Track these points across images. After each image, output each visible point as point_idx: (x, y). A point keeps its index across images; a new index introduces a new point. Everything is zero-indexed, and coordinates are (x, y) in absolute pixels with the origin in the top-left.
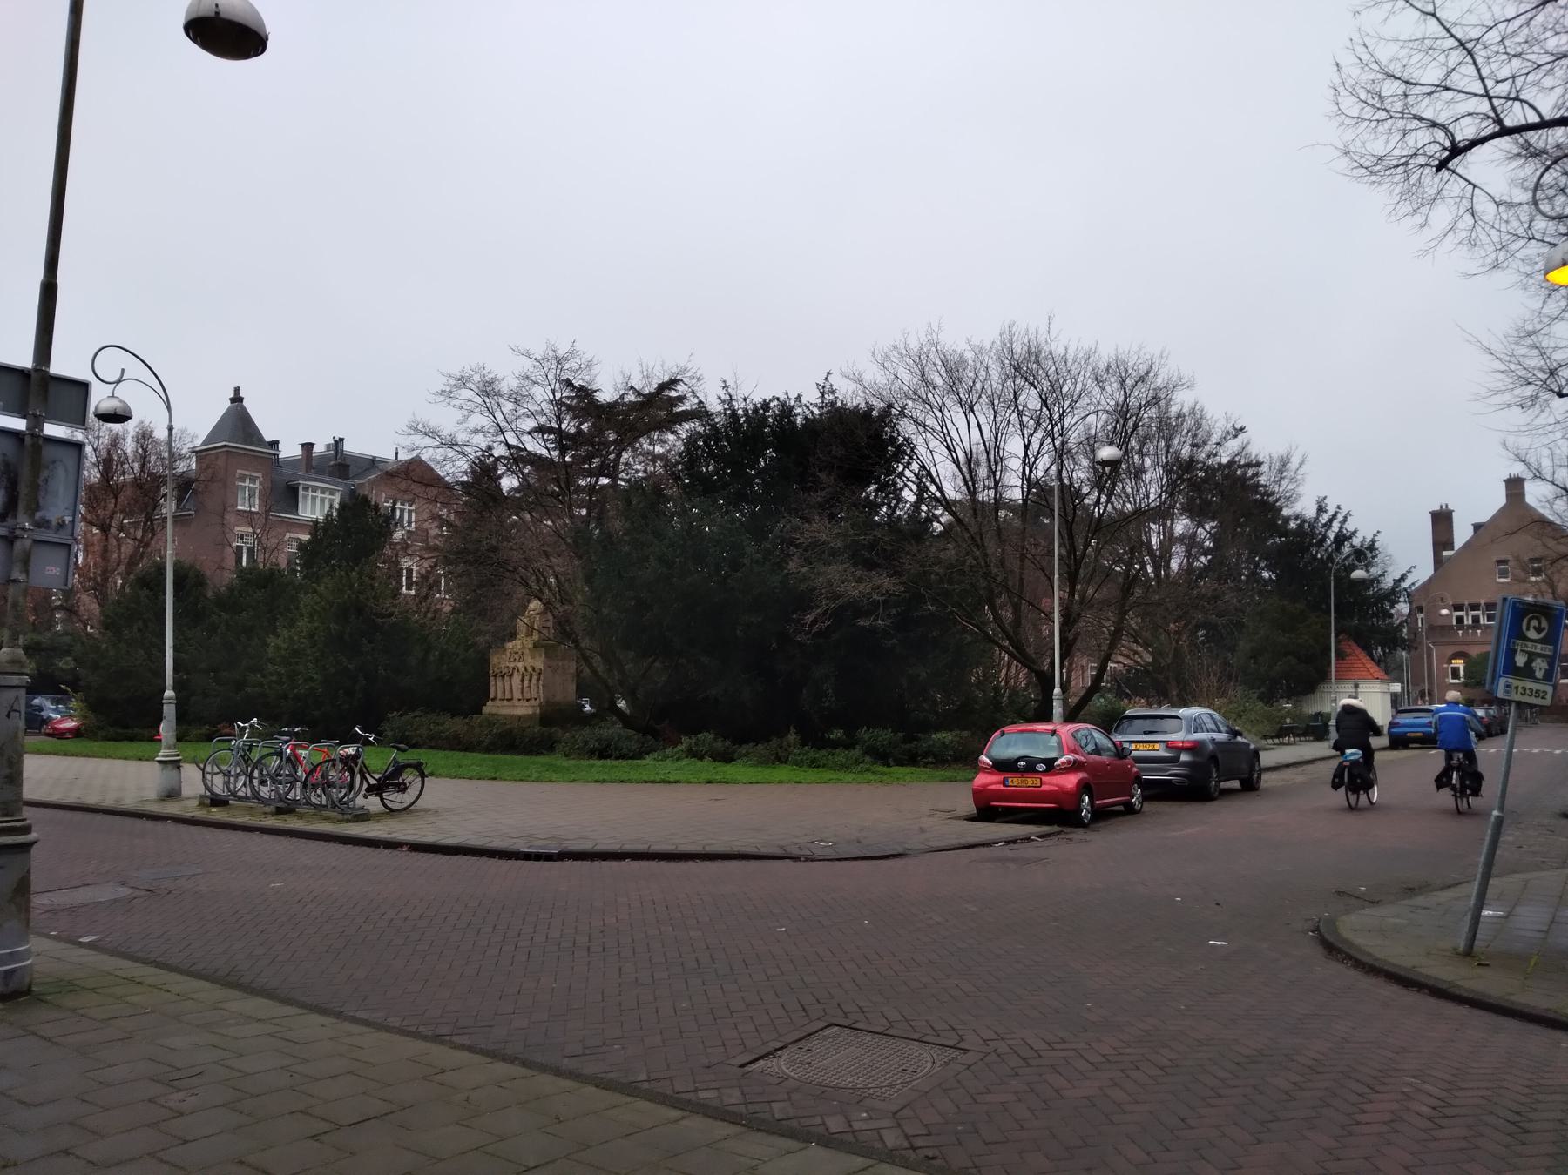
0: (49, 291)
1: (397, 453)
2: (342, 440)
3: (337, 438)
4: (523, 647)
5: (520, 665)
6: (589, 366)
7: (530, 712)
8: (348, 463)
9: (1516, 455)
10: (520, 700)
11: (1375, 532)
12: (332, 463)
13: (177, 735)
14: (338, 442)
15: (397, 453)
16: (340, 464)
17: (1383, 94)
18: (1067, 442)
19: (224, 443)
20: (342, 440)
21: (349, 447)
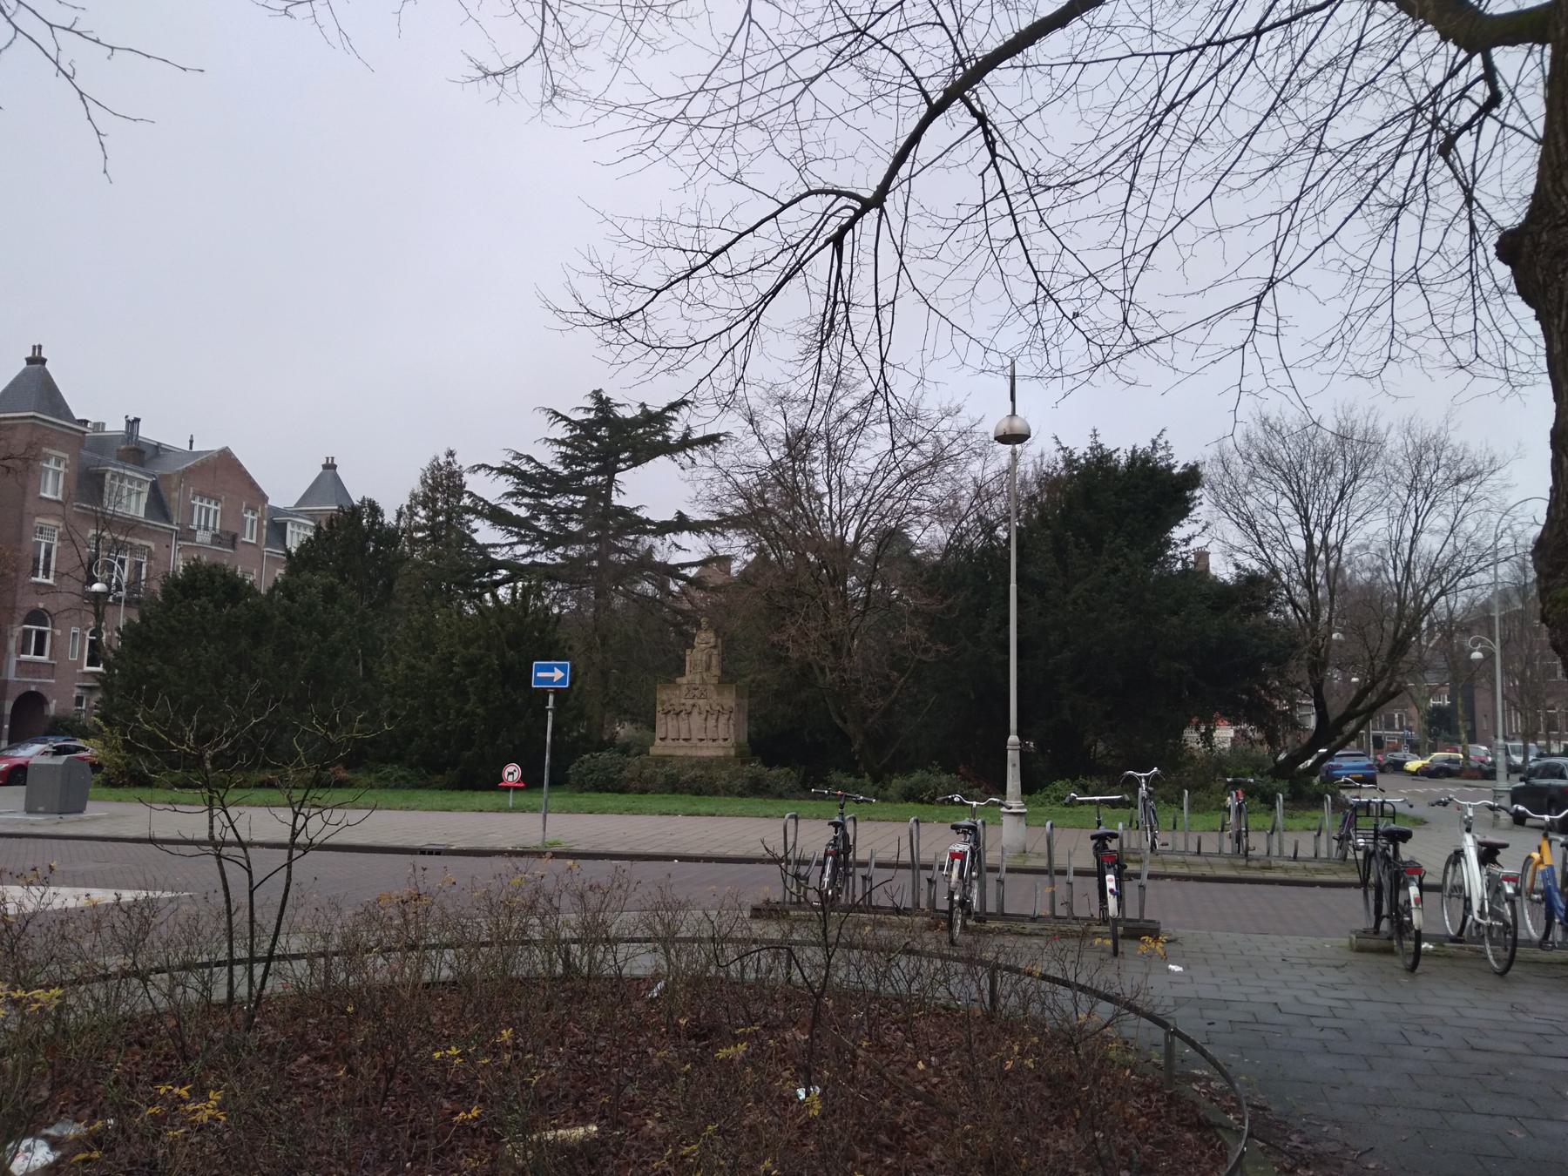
0: (1013, 399)
1: (191, 442)
2: (137, 420)
3: (131, 418)
4: (704, 683)
5: (701, 702)
6: (1465, 450)
7: (721, 753)
8: (142, 447)
9: (846, 414)
10: (701, 740)
11: (113, 58)
12: (123, 447)
13: (66, 719)
14: (133, 423)
15: (191, 442)
16: (135, 449)
17: (1353, 910)
18: (1338, 568)
19: (32, 414)
20: (137, 420)
21: (146, 433)
